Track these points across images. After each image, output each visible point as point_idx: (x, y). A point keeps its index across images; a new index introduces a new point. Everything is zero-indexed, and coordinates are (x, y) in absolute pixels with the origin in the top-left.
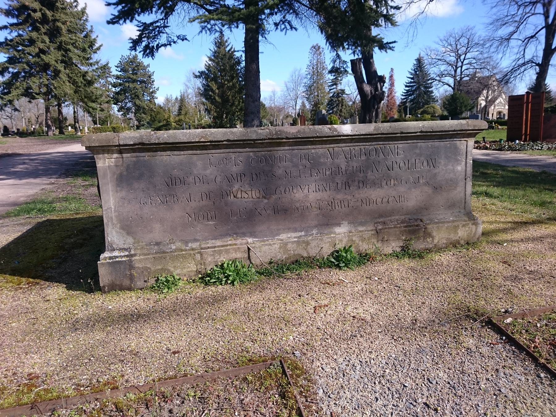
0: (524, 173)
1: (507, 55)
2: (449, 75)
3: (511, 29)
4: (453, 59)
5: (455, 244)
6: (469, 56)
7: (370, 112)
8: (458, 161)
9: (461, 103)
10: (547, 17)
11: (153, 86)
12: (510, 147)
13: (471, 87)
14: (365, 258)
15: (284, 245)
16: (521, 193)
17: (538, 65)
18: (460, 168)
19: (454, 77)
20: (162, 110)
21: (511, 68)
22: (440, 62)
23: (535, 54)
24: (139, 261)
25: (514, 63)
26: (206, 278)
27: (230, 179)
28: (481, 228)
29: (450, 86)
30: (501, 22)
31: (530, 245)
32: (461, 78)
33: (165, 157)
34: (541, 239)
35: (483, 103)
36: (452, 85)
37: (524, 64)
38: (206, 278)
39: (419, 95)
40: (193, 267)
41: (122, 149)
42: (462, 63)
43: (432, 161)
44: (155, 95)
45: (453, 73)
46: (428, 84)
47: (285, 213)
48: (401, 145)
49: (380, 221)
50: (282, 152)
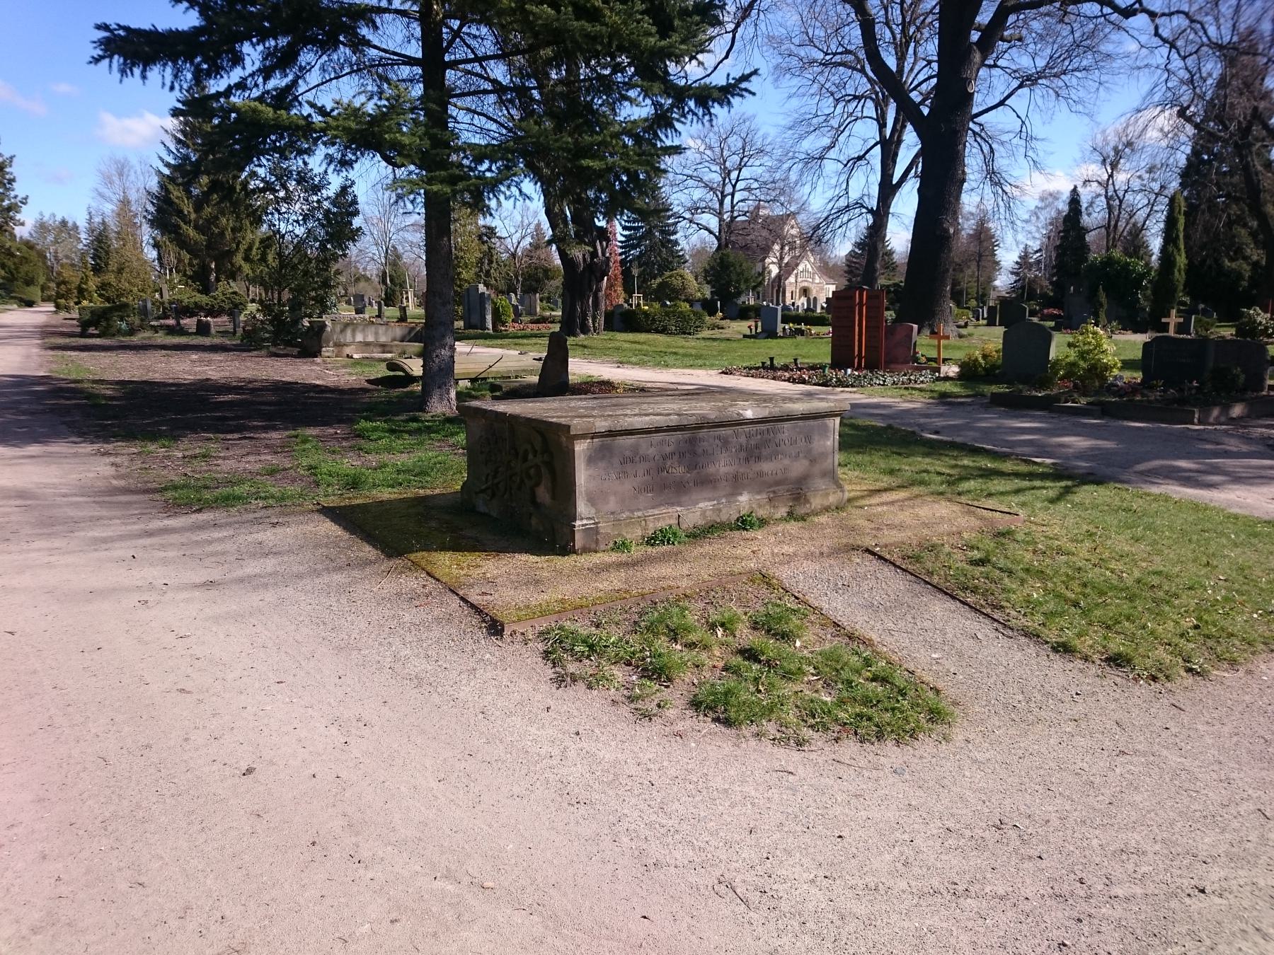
0: (865, 428)
1: (819, 189)
2: (707, 209)
3: (826, 141)
4: (717, 178)
5: (827, 509)
6: (745, 173)
7: (584, 299)
8: (827, 438)
9: (738, 274)
10: (882, 126)
11: (12, 194)
12: (839, 380)
13: (752, 237)
14: (763, 522)
15: (704, 512)
16: (867, 458)
17: (870, 211)
18: (829, 443)
19: (719, 214)
20: (33, 253)
21: (825, 214)
22: (690, 182)
23: (866, 191)
24: (604, 527)
25: (830, 205)
26: (651, 541)
27: (664, 458)
28: (847, 495)
29: (711, 232)
30: (804, 125)
31: (885, 508)
32: (733, 218)
33: (621, 441)
34: (892, 503)
35: (775, 270)
36: (716, 231)
37: (848, 208)
38: (651, 541)
39: (651, 248)
40: (639, 533)
41: (594, 436)
42: (734, 186)
43: (809, 439)
44: (18, 217)
45: (717, 206)
46: (669, 225)
47: (707, 483)
48: (787, 425)
49: (771, 487)
50: (703, 433)
